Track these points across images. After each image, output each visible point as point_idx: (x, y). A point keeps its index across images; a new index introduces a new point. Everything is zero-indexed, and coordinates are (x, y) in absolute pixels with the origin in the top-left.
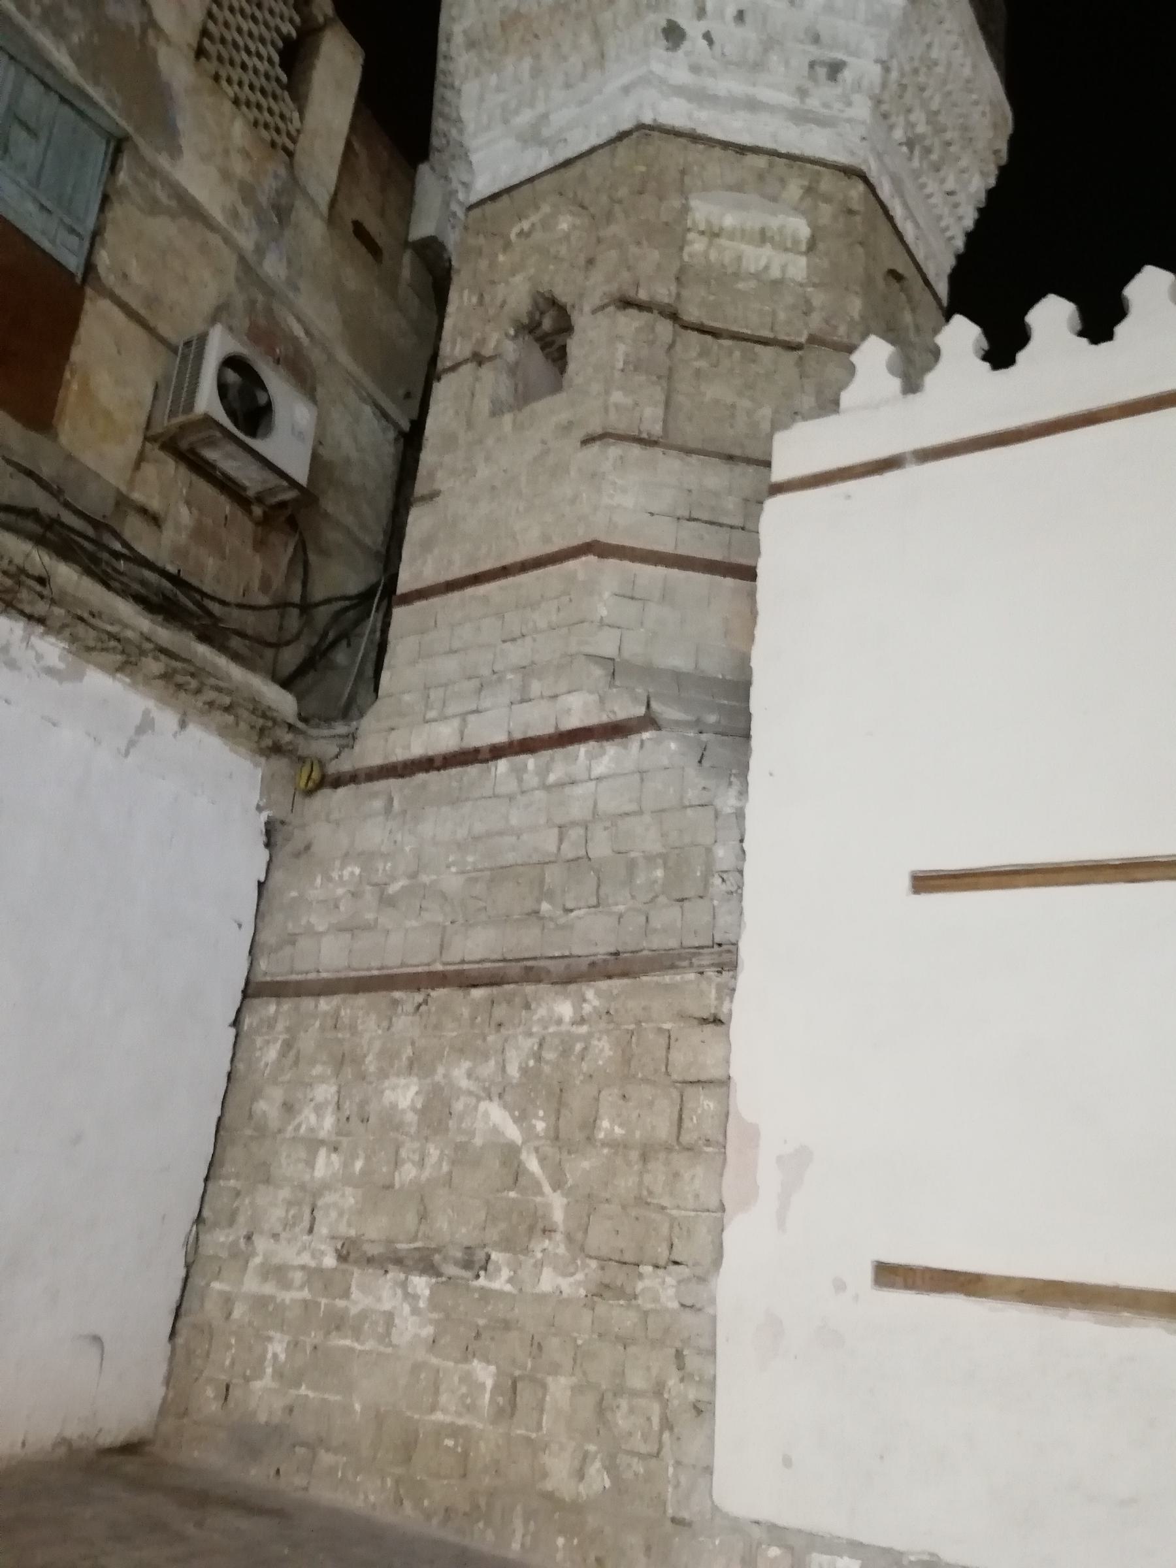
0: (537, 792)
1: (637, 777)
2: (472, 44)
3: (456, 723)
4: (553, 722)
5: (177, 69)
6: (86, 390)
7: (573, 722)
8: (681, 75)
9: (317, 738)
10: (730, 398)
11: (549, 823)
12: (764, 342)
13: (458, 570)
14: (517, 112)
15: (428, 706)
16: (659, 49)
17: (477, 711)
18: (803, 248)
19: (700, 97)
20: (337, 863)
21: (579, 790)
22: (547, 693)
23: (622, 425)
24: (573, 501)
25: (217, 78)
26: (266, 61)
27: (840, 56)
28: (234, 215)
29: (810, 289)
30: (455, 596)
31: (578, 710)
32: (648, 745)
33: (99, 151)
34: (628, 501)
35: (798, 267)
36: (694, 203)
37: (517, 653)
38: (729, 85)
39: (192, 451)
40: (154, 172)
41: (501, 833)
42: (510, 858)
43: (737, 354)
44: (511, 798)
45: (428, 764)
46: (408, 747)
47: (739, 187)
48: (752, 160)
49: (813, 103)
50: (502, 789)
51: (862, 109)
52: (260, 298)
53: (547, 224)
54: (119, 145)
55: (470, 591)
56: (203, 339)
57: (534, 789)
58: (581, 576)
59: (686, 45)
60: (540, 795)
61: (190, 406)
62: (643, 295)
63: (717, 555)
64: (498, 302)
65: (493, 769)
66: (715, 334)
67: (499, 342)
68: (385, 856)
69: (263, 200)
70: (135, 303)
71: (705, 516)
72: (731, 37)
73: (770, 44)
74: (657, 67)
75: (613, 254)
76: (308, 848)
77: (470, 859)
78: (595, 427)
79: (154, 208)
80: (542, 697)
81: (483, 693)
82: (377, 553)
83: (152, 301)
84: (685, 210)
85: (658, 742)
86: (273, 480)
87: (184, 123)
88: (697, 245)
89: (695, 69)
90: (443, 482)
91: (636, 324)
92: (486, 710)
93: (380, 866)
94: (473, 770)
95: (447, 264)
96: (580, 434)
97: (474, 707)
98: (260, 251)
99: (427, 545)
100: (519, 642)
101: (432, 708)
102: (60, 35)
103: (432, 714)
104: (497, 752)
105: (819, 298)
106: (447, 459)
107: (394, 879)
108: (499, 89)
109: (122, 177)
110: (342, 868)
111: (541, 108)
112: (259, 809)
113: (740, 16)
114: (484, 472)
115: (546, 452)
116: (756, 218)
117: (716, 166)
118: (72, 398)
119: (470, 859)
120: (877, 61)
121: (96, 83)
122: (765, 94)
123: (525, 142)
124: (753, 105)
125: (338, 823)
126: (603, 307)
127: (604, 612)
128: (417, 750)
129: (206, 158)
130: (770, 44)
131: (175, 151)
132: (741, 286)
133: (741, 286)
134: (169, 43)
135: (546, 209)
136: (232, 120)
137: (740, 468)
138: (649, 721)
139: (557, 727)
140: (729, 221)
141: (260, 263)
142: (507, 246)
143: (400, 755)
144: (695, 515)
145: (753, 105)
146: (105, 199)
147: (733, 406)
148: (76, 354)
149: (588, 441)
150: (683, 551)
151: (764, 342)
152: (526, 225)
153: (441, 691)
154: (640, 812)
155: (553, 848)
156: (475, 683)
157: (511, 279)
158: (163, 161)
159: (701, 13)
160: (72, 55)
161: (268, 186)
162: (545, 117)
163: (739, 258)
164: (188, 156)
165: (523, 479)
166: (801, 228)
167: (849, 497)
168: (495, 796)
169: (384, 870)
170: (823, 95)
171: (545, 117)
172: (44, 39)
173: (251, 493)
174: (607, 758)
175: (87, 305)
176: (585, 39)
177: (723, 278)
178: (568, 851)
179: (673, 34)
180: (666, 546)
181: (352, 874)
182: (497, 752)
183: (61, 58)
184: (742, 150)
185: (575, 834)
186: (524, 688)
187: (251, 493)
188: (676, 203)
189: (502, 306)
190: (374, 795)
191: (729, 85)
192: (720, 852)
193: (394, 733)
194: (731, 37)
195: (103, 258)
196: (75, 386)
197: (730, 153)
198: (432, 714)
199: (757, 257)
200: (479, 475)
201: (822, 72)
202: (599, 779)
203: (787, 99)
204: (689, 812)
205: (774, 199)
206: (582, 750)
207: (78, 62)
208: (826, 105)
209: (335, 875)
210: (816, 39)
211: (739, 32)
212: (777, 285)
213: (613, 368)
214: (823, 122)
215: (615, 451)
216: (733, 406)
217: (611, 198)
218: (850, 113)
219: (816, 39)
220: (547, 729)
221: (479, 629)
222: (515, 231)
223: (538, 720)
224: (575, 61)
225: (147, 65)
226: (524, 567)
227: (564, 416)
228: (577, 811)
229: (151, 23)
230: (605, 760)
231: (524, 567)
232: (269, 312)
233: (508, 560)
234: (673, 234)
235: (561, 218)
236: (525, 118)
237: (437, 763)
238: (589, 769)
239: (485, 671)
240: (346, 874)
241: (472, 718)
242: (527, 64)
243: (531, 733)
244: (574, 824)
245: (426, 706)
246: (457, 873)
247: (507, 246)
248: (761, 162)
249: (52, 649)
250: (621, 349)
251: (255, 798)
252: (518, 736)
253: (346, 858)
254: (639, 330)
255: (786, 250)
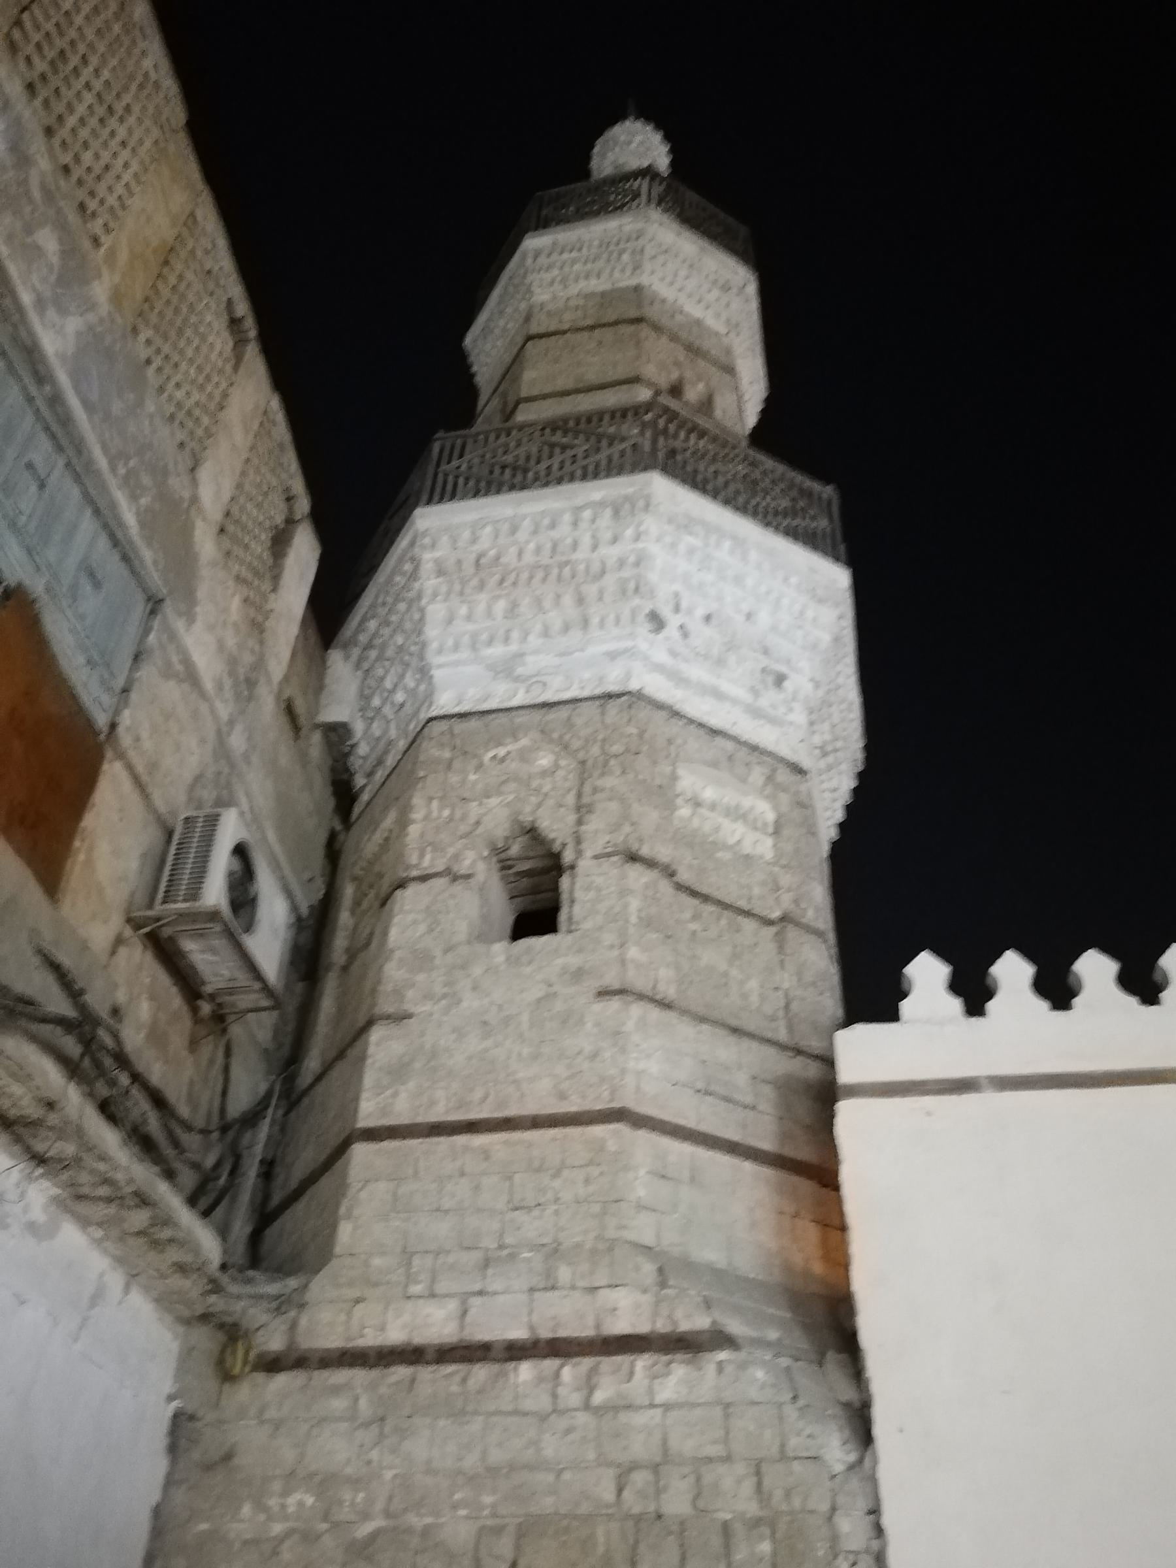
0: (579, 1414)
1: (718, 1411)
2: (441, 572)
3: (453, 1305)
4: (590, 1321)
5: (206, 545)
6: (89, 862)
7: (621, 1326)
8: (661, 656)
9: (239, 1297)
10: (723, 966)
11: (603, 1461)
12: (748, 914)
13: (439, 1113)
14: (490, 642)
15: (410, 1279)
16: (643, 628)
17: (481, 1293)
18: (771, 830)
19: (679, 679)
20: (277, 1486)
21: (640, 1419)
22: (581, 1284)
23: (640, 983)
24: (594, 1056)
25: (228, 554)
26: (260, 547)
27: (783, 669)
28: (220, 687)
29: (776, 869)
30: (443, 1143)
31: (628, 1312)
32: (729, 1369)
33: (140, 608)
34: (653, 1066)
35: (765, 847)
36: (681, 772)
37: (531, 1227)
38: (697, 672)
39: (171, 939)
40: (173, 637)
41: (531, 1467)
42: (548, 1504)
43: (723, 922)
44: (543, 1418)
45: (412, 1355)
46: (382, 1328)
47: (714, 764)
48: (719, 741)
49: (764, 702)
50: (528, 1405)
51: (799, 717)
52: (226, 770)
53: (524, 756)
54: (155, 604)
55: (461, 1140)
56: (212, 821)
57: (576, 1410)
58: (611, 1146)
59: (665, 633)
60: (582, 1418)
61: (194, 893)
62: (645, 851)
63: (732, 1134)
64: (472, 819)
65: (512, 1375)
66: (706, 898)
67: (474, 862)
68: (356, 1483)
69: (241, 671)
70: (140, 769)
71: (722, 1091)
72: (703, 635)
73: (731, 646)
74: (643, 646)
75: (614, 806)
76: (228, 1457)
77: (488, 1499)
78: (611, 979)
79: (168, 673)
80: (573, 1287)
81: (490, 1271)
82: (266, 1050)
83: (153, 766)
84: (674, 778)
85: (743, 1366)
86: (243, 978)
87: (202, 593)
88: (684, 812)
89: (673, 654)
90: (412, 1001)
91: (644, 880)
92: (495, 1293)
93: (347, 1496)
94: (481, 1373)
95: (347, 749)
96: (595, 984)
97: (477, 1287)
98: (231, 723)
99: (398, 1072)
100: (536, 1213)
101: (418, 1282)
102: (134, 497)
103: (416, 1289)
104: (516, 1352)
105: (786, 879)
106: (421, 977)
107: (366, 1516)
108: (469, 618)
109: (152, 638)
110: (286, 1493)
111: (514, 647)
112: (171, 1398)
113: (708, 618)
114: (470, 1002)
115: (550, 996)
116: (730, 797)
117: (694, 743)
118: (78, 868)
119: (488, 1499)
120: (812, 680)
121: (149, 545)
122: (726, 687)
123: (497, 673)
124: (719, 695)
125: (278, 1425)
126: (609, 855)
127: (641, 1192)
128: (395, 1335)
129: (211, 628)
130: (731, 646)
131: (191, 619)
132: (719, 855)
133: (719, 855)
134: (204, 519)
135: (524, 742)
136: (233, 595)
137: (746, 1043)
138: (720, 1339)
139: (598, 1326)
140: (709, 794)
141: (229, 734)
142: (480, 767)
143: (370, 1339)
144: (712, 1088)
145: (719, 695)
146: (137, 657)
147: (725, 974)
148: (89, 820)
149: (604, 993)
150: (704, 1127)
151: (748, 914)
152: (502, 751)
153: (429, 1260)
154: (728, 1459)
155: (609, 1496)
156: (476, 1256)
157: (485, 801)
158: (180, 625)
159: (677, 609)
160: (138, 514)
161: (248, 659)
162: (520, 655)
163: (717, 829)
164: (198, 626)
165: (525, 1018)
166: (766, 811)
167: (929, 1114)
168: (515, 1412)
169: (353, 1504)
170: (769, 698)
171: (520, 655)
172: (121, 497)
173: (208, 989)
174: (675, 1380)
175: (106, 767)
176: (568, 600)
177: (704, 846)
178: (632, 1502)
179: (657, 622)
180: (689, 1121)
181: (301, 1504)
182: (516, 1352)
183: (130, 518)
184: (715, 732)
185: (640, 1478)
186: (549, 1273)
187: (208, 989)
188: (668, 769)
189: (478, 823)
190: (336, 1390)
191: (697, 672)
192: (845, 1525)
193: (361, 1306)
194: (703, 635)
195: (126, 718)
196: (82, 857)
197: (702, 732)
198: (416, 1289)
199: (733, 832)
200: (465, 1004)
201: (770, 679)
202: (667, 1407)
203: (741, 693)
204: (797, 1466)
205: (744, 780)
206: (642, 1362)
207: (142, 524)
208: (774, 707)
209: (273, 1502)
210: (766, 652)
211: (708, 632)
212: (748, 859)
213: (627, 921)
214: (773, 721)
215: (637, 1010)
216: (725, 974)
217: (604, 753)
218: (791, 717)
219: (766, 652)
220: (585, 1330)
221: (477, 1188)
222: (491, 754)
223: (567, 1315)
224: (555, 618)
225: (186, 532)
226: (536, 1122)
227: (574, 961)
228: (640, 1448)
229: (195, 500)
230: (672, 1380)
231: (536, 1122)
232: (229, 785)
233: (512, 1111)
234: (664, 795)
235: (542, 753)
236: (497, 651)
237: (430, 1356)
238: (651, 1392)
239: (490, 1243)
240: (292, 1501)
241: (476, 1301)
242: (501, 606)
243: (562, 1333)
244: (634, 1467)
245: (408, 1275)
246: (467, 1517)
247: (480, 767)
248: (729, 746)
249: (40, 1194)
250: (635, 904)
251: (168, 1387)
252: (545, 1334)
253: (291, 1481)
254: (647, 886)
255: (755, 829)
